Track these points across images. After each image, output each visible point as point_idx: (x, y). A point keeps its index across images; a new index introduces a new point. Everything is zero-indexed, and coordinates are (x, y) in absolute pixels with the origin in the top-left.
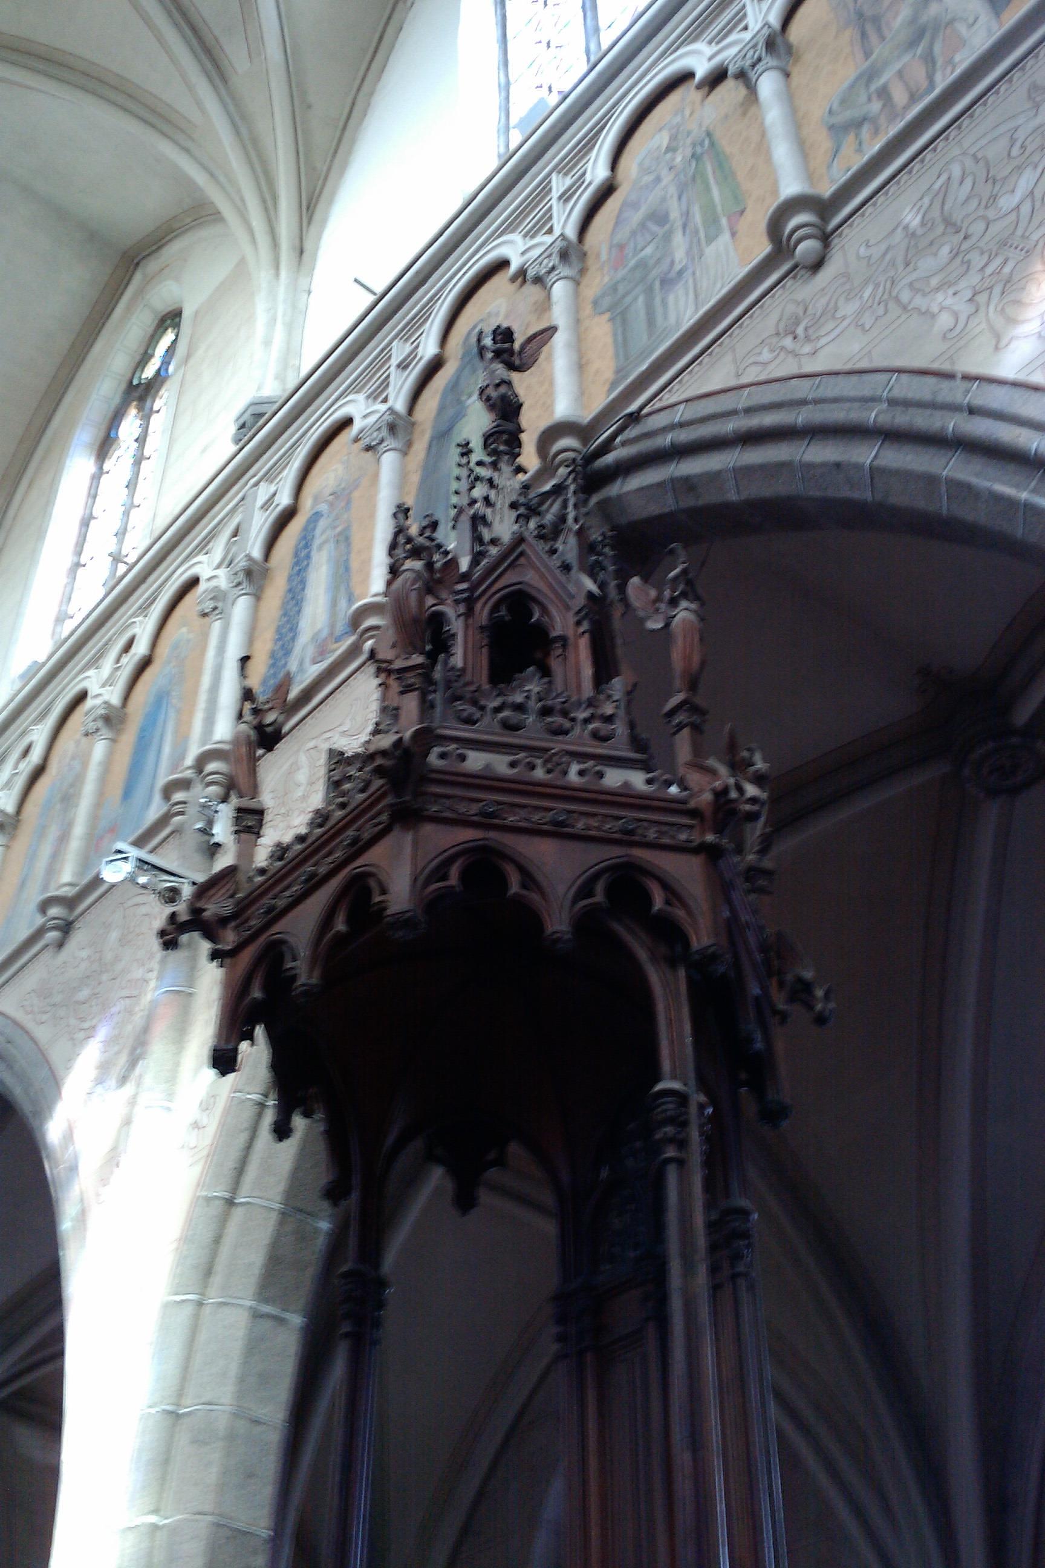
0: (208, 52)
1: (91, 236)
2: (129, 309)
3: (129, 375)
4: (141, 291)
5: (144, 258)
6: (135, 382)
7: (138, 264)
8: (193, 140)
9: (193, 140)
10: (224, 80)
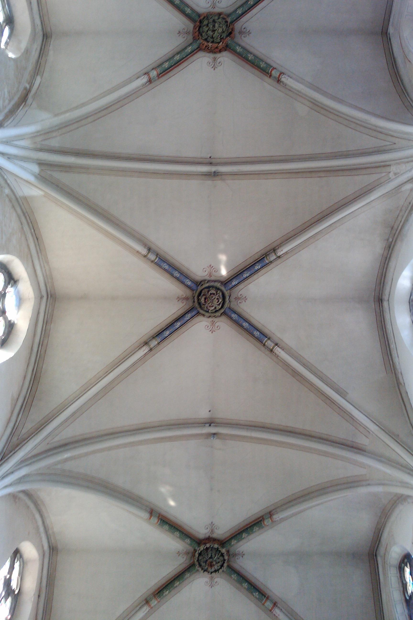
0: (352, 447)
1: (354, 555)
2: (384, 574)
3: (403, 598)
4: (384, 563)
5: (376, 551)
6: (408, 598)
7: (376, 555)
8: (368, 480)
9: (368, 480)
10: (364, 451)
